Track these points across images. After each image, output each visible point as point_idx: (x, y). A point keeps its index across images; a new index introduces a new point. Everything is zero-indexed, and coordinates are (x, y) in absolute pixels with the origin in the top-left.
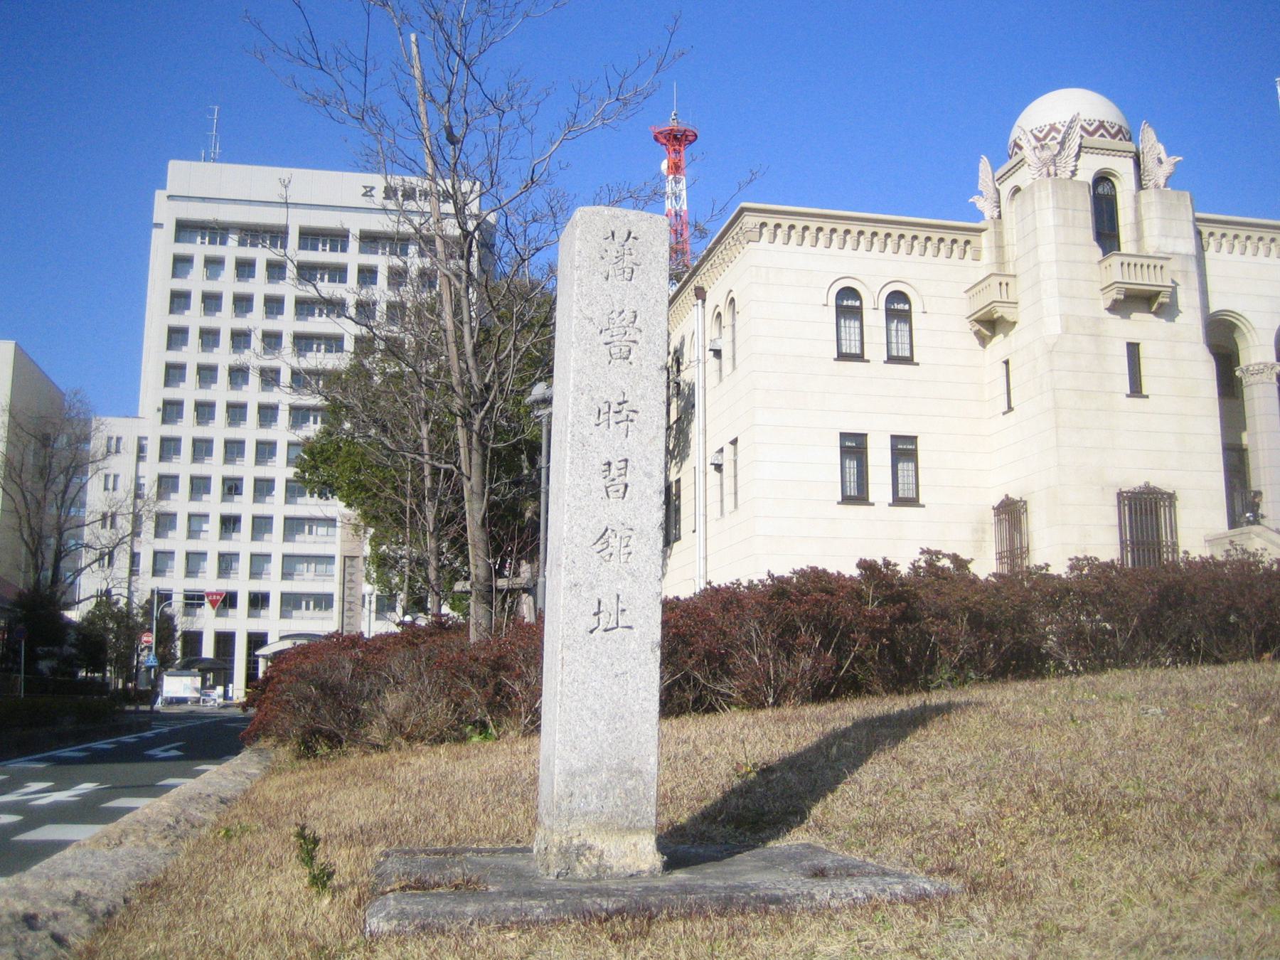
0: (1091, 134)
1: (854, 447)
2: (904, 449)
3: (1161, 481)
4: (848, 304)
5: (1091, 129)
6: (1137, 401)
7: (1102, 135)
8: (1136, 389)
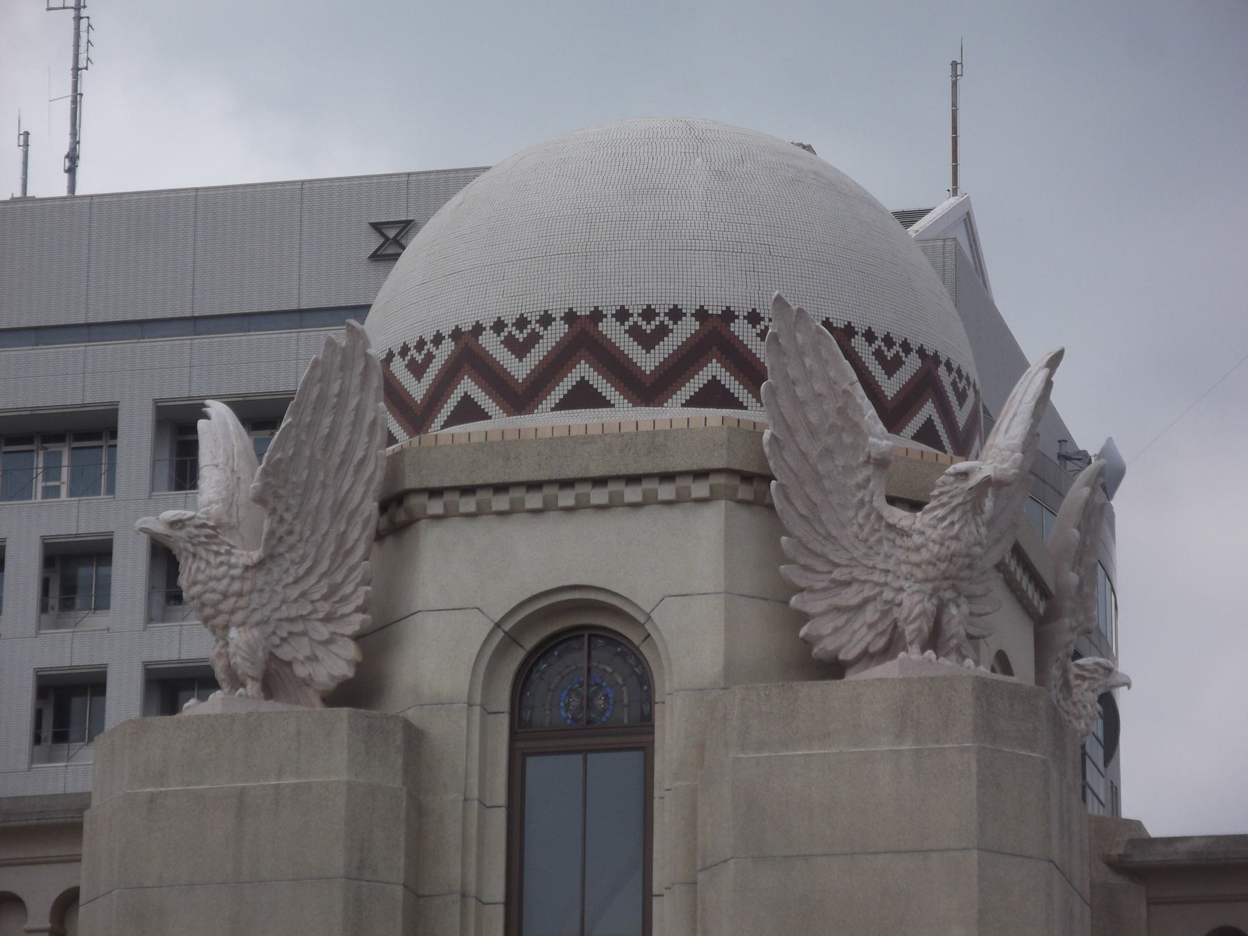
5: (648, 361)
7: (584, 397)
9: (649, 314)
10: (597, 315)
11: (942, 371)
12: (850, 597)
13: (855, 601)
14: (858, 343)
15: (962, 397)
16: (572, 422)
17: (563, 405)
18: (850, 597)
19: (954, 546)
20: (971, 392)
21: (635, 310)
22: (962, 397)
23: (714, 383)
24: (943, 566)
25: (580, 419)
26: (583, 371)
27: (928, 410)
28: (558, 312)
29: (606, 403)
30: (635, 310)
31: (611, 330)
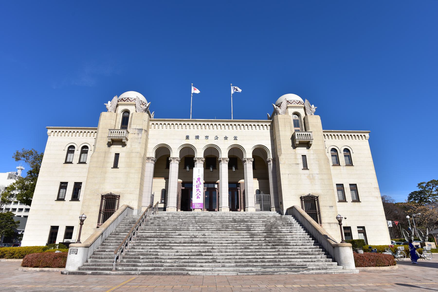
0: (298, 104)
1: (63, 185)
2: (354, 187)
3: (114, 191)
4: (71, 149)
6: (115, 170)
8: (116, 166)
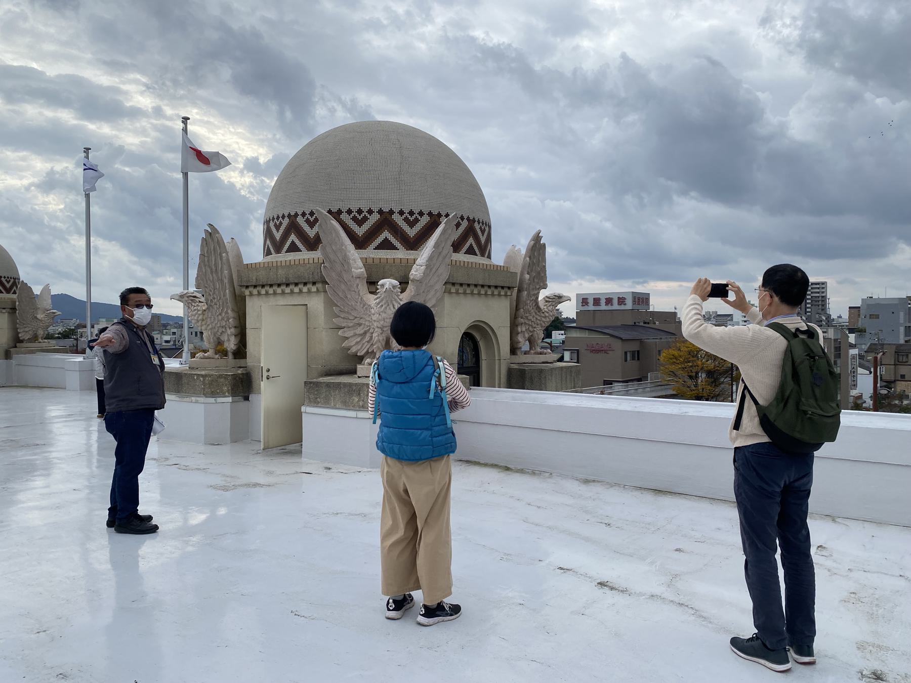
7: (386, 245)
9: (360, 211)
10: (391, 212)
11: (476, 224)
12: (27, 329)
13: (362, 332)
14: (344, 217)
15: (483, 232)
16: (388, 257)
17: (378, 248)
18: (27, 329)
19: (384, 315)
20: (487, 229)
21: (354, 210)
22: (483, 232)
23: (386, 240)
24: (382, 323)
25: (292, 256)
26: (386, 234)
27: (471, 241)
28: (426, 211)
29: (395, 248)
30: (354, 210)
31: (396, 218)
